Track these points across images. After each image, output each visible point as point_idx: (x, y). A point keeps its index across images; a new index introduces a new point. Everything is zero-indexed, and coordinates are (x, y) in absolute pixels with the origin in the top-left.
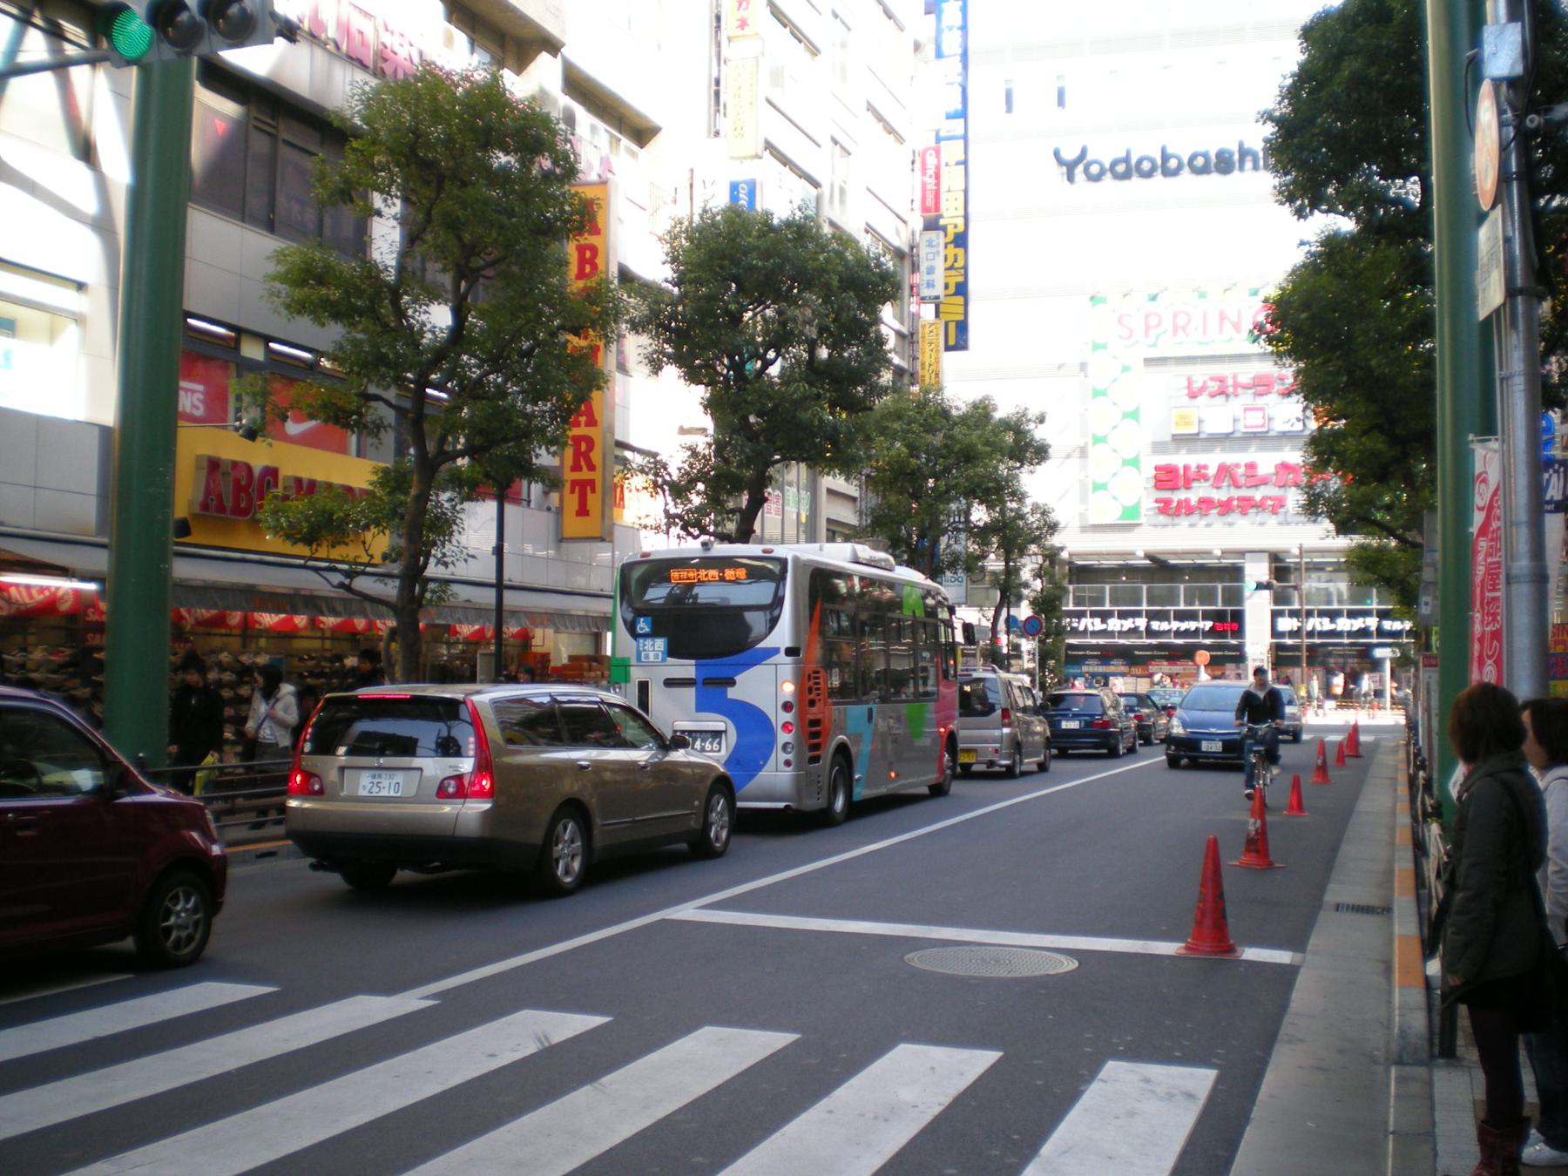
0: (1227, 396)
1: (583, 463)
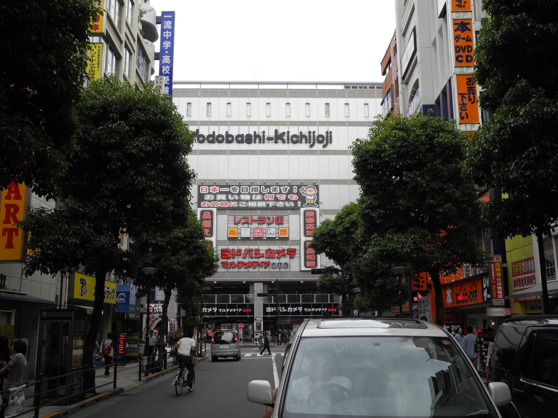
0: (248, 224)
1: (11, 219)
